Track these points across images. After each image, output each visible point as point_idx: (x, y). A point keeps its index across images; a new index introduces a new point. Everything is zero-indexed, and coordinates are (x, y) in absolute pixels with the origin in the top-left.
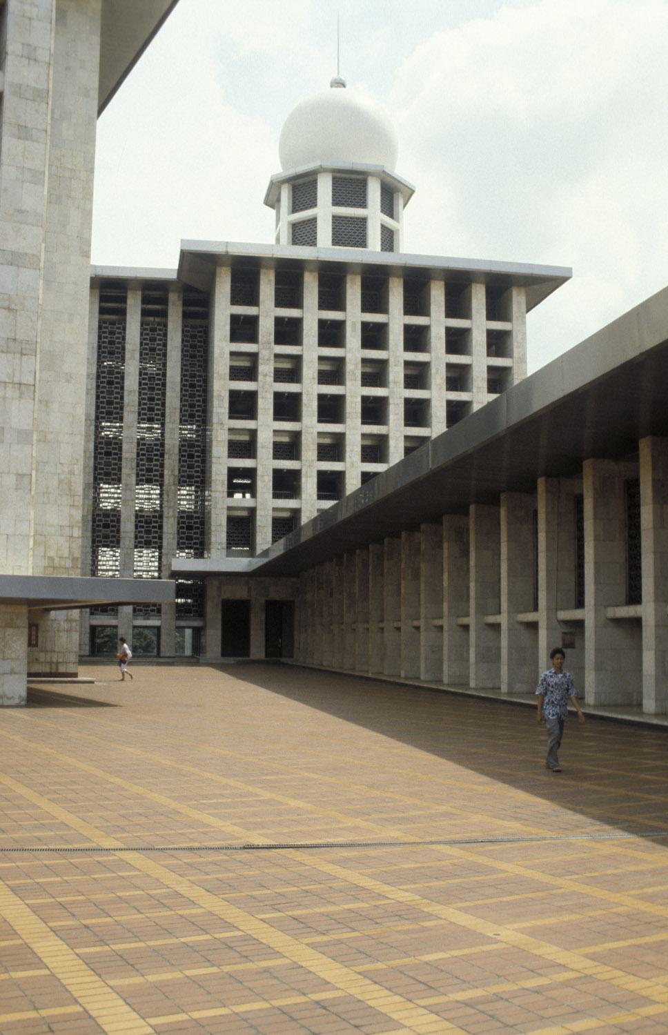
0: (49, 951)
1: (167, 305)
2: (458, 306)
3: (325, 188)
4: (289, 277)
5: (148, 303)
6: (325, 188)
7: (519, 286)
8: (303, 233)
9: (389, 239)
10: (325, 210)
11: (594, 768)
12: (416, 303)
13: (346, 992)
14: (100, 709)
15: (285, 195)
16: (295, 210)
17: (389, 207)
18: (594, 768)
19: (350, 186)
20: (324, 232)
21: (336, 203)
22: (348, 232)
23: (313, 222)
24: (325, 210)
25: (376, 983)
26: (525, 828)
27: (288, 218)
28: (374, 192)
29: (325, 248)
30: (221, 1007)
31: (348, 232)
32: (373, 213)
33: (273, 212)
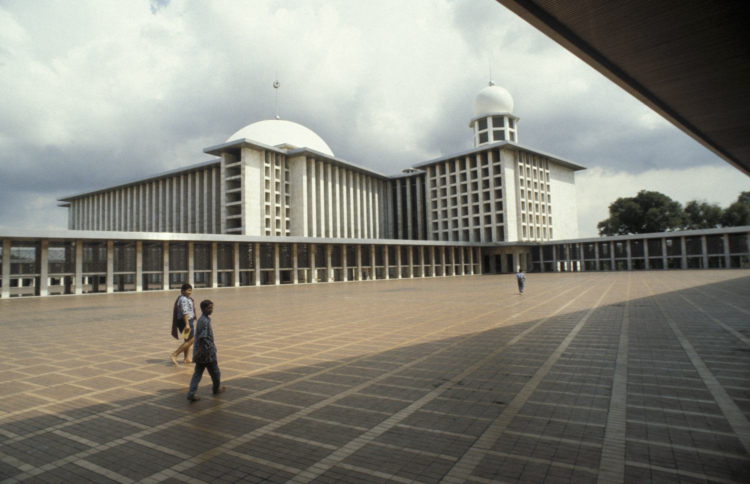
0: (88, 222)
2: (485, 162)
3: (490, 122)
4: (484, 154)
5: (152, 229)
6: (490, 122)
8: (484, 138)
10: (490, 129)
13: (14, 440)
14: (60, 199)
15: (476, 124)
17: (511, 126)
19: (498, 120)
21: (494, 126)
22: (499, 135)
23: (486, 133)
24: (490, 129)
25: (21, 435)
28: (507, 123)
29: (492, 142)
30: (38, 475)
32: (507, 129)
33: (473, 129)
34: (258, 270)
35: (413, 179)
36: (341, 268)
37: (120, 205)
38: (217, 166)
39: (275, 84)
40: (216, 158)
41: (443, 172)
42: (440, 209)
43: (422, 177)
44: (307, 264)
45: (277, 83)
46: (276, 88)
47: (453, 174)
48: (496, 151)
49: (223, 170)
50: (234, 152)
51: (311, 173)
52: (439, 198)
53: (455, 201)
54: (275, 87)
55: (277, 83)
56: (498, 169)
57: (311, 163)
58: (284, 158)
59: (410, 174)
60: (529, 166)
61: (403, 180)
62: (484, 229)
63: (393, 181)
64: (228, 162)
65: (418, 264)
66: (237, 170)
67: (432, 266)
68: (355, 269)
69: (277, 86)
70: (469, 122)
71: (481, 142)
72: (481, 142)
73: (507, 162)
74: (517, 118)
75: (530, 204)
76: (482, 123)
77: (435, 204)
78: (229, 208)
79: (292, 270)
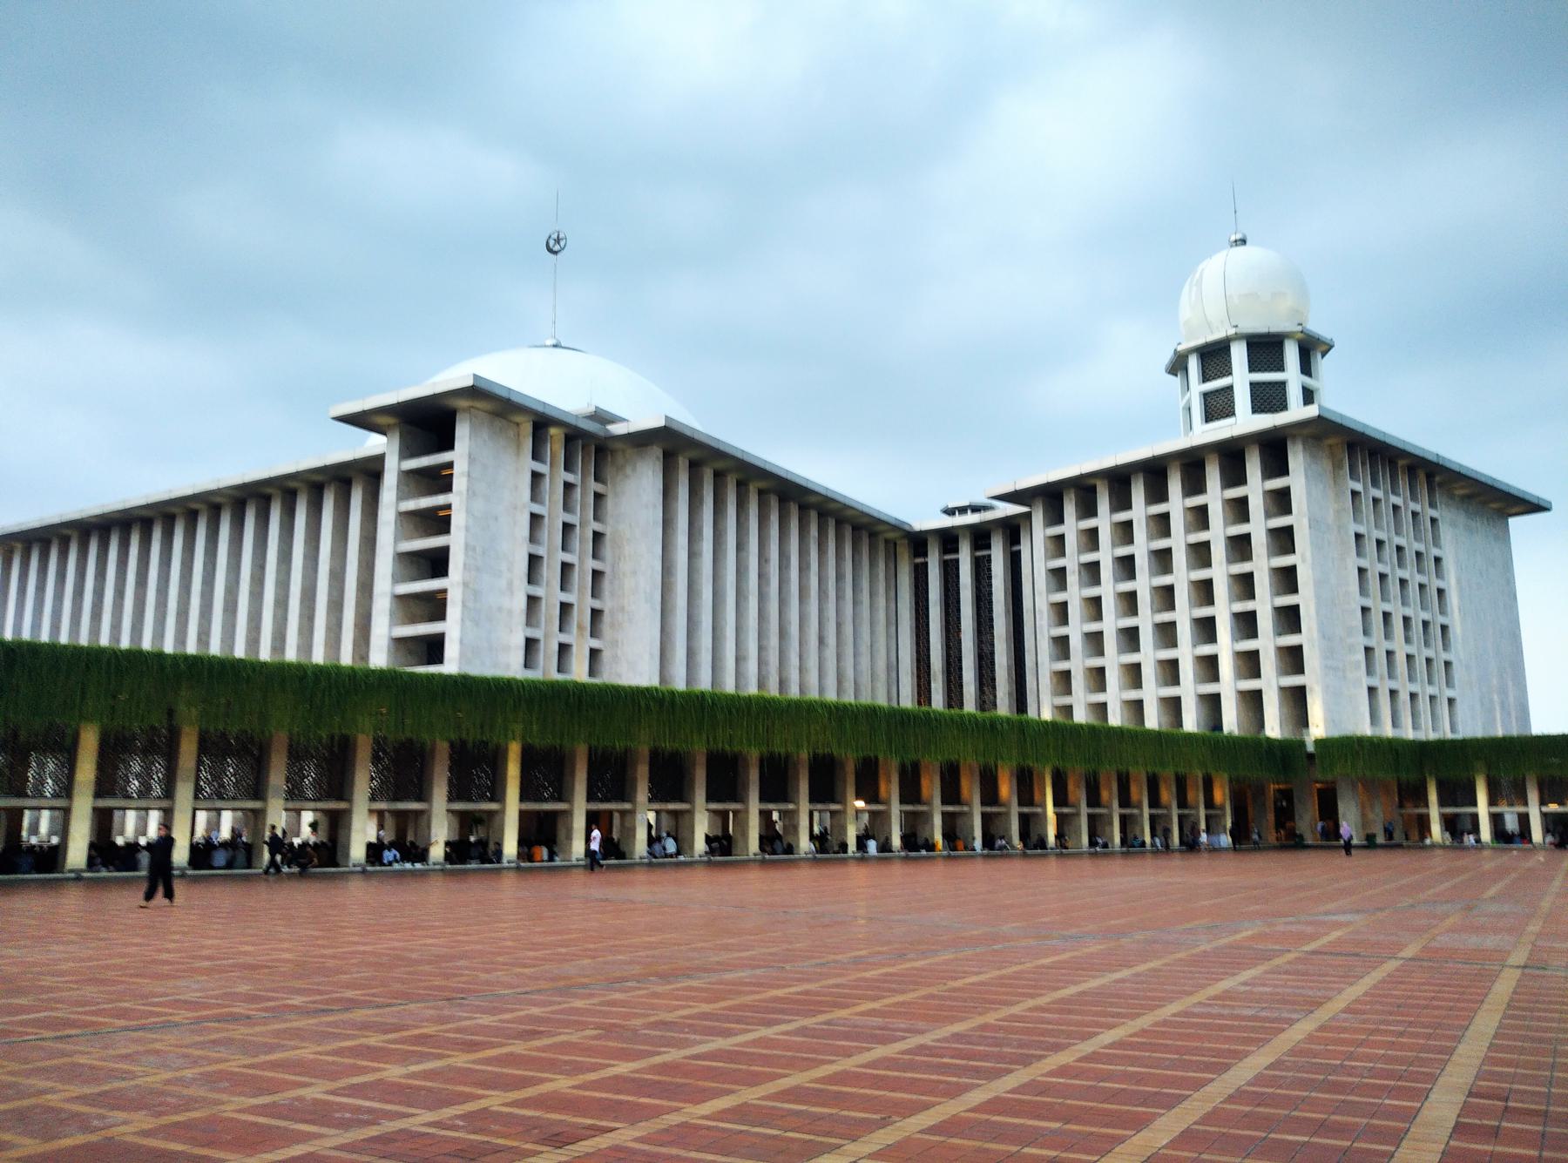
1: (350, 800)
3: (1239, 354)
4: (1231, 455)
6: (1239, 354)
7: (1294, 437)
8: (1218, 405)
9: (1308, 396)
10: (1241, 377)
11: (94, 1019)
12: (1195, 484)
15: (1193, 364)
16: (1205, 378)
18: (94, 1019)
19: (1265, 349)
20: (1242, 399)
21: (1253, 368)
24: (1241, 377)
26: (1507, 881)
27: (1198, 387)
28: (1291, 354)
29: (1245, 421)
31: (1268, 398)
33: (1176, 381)
34: (1434, 812)
35: (980, 536)
36: (493, 806)
37: (59, 597)
38: (371, 470)
39: (552, 243)
40: (374, 443)
41: (1088, 510)
42: (1076, 630)
43: (1013, 530)
44: (622, 791)
45: (558, 241)
46: (555, 253)
47: (1122, 516)
48: (1274, 449)
49: (390, 480)
50: (427, 423)
51: (676, 498)
52: (1075, 594)
53: (1129, 602)
54: (550, 250)
55: (558, 241)
56: (1281, 501)
57: (676, 468)
58: (590, 448)
59: (971, 518)
60: (1379, 494)
61: (948, 539)
62: (1118, 705)
63: (918, 542)
64: (407, 452)
65: (1031, 803)
66: (439, 480)
67: (1078, 814)
68: (735, 813)
69: (557, 248)
70: (1167, 357)
71: (1210, 416)
72: (1210, 416)
73: (1302, 475)
74: (1324, 343)
75: (1386, 616)
76: (1214, 356)
77: (1061, 612)
78: (402, 600)
79: (1073, 815)
